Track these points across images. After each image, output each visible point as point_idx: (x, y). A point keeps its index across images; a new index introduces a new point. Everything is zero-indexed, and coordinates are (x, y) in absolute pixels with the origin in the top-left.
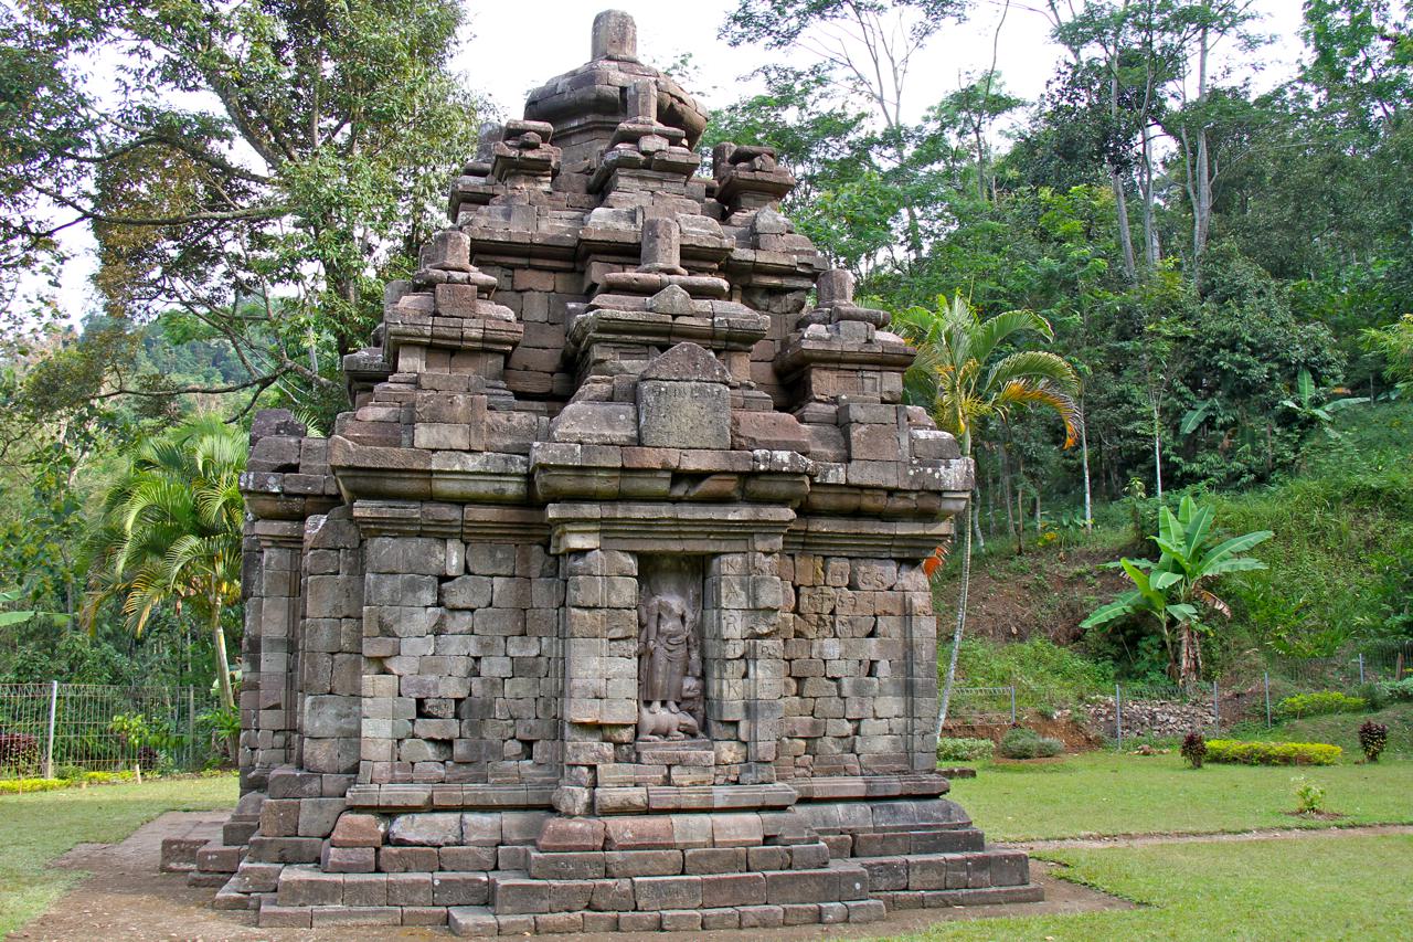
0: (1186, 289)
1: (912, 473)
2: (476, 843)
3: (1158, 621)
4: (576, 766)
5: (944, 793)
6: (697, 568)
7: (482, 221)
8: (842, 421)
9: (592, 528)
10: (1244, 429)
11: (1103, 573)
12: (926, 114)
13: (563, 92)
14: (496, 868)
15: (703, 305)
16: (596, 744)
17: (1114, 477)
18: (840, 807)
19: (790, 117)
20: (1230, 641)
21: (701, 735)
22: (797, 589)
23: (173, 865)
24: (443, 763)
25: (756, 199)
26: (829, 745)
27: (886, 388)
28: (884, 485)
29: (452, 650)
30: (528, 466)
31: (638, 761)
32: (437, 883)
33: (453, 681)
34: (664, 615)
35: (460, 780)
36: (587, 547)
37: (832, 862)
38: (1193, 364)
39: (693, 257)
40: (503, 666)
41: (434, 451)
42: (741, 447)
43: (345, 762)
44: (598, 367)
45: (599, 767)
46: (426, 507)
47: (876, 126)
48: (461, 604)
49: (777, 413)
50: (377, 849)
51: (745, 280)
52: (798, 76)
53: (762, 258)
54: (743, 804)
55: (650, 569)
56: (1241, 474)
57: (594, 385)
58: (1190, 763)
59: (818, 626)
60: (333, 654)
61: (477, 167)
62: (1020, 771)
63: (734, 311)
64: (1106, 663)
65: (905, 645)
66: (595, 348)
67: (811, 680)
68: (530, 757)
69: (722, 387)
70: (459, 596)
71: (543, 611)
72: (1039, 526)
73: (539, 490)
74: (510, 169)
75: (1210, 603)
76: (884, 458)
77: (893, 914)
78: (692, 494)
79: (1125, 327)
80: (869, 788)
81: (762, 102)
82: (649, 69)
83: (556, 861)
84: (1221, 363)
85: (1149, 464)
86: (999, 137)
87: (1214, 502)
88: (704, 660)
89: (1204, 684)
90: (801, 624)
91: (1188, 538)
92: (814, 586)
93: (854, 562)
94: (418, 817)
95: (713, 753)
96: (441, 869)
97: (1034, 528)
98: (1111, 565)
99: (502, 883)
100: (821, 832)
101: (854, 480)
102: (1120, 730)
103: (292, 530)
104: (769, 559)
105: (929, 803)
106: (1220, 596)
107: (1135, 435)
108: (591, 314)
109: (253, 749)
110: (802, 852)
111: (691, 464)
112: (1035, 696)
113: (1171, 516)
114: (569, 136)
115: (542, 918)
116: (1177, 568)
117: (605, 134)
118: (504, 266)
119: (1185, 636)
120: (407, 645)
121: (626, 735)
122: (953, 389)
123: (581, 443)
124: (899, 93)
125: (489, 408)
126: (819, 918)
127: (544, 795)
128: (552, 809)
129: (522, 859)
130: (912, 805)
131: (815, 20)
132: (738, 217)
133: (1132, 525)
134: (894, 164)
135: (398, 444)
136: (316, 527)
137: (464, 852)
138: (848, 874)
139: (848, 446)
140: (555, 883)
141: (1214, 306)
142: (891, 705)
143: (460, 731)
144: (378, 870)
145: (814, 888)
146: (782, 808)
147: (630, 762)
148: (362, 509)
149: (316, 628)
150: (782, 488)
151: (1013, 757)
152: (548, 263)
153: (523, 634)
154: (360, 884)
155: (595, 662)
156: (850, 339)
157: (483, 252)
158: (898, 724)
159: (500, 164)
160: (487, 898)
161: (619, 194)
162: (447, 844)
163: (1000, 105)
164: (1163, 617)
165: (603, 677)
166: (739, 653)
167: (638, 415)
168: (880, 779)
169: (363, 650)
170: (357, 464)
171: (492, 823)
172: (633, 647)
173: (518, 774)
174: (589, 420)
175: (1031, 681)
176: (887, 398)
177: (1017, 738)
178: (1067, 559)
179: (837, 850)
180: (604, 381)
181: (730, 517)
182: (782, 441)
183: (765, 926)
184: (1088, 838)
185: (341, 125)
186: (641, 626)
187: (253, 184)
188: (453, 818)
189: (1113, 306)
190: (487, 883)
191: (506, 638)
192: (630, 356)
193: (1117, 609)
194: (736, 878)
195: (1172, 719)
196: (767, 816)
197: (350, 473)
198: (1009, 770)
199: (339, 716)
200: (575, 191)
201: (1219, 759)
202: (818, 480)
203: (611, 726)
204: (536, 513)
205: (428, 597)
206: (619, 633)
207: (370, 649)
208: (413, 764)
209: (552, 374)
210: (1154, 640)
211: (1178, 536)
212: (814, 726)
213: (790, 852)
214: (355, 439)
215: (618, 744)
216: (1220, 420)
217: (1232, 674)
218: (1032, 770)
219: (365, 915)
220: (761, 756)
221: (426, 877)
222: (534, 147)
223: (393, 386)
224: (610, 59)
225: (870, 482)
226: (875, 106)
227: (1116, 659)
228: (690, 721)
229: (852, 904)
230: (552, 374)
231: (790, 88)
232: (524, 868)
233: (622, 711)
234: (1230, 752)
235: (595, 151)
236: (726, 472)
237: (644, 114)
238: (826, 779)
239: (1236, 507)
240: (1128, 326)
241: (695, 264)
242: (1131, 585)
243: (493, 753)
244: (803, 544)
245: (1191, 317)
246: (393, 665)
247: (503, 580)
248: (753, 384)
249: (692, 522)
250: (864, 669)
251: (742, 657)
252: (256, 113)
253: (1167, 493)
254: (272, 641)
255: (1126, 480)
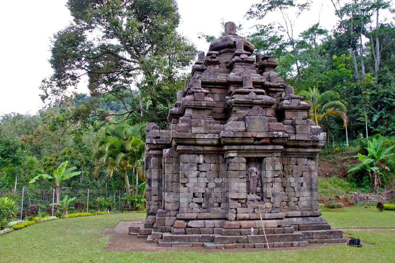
0: (373, 81)
1: (311, 136)
2: (208, 227)
3: (368, 172)
4: (232, 209)
5: (320, 215)
6: (259, 161)
7: (203, 77)
8: (293, 124)
9: (235, 151)
10: (391, 119)
11: (352, 159)
12: (300, 35)
13: (220, 43)
14: (213, 233)
15: (260, 96)
16: (237, 204)
17: (354, 132)
18: (295, 219)
19: (264, 38)
20: (389, 177)
21: (261, 201)
22: (283, 165)
23: (132, 233)
24: (199, 208)
25: (269, 69)
26: (291, 203)
27: (304, 115)
28: (304, 140)
29: (201, 181)
30: (219, 137)
31: (247, 207)
32: (200, 237)
33: (202, 189)
34: (252, 172)
35: (204, 212)
36: (234, 156)
37: (294, 232)
38: (376, 101)
39: (256, 84)
40: (213, 185)
41: (197, 133)
42: (270, 131)
43: (176, 208)
44: (234, 112)
45: (238, 209)
46: (195, 147)
47: (286, 39)
48: (203, 170)
49: (278, 123)
50: (185, 229)
51: (269, 90)
52: (265, 27)
53: (271, 84)
54: (272, 218)
55: (249, 161)
56: (391, 131)
57: (233, 117)
58: (379, 210)
59: (289, 174)
60: (172, 182)
61: (199, 62)
62: (332, 211)
63: (266, 98)
64: (354, 183)
65: (310, 179)
66: (234, 108)
67: (287, 187)
68: (220, 207)
69: (265, 117)
70: (203, 168)
71: (223, 172)
72: (334, 146)
73: (222, 142)
74: (208, 63)
75: (383, 167)
76: (304, 133)
77: (310, 245)
78: (259, 143)
79: (356, 92)
80: (302, 214)
81: (258, 34)
82: (240, 37)
83: (229, 231)
84: (384, 101)
85: (364, 129)
86: (319, 40)
87: (383, 139)
88: (261, 183)
89: (382, 189)
90: (285, 174)
91: (376, 149)
92: (287, 165)
93: (297, 159)
94: (194, 221)
95: (265, 206)
96: (200, 233)
97: (332, 147)
98: (354, 156)
99: (216, 236)
100: (292, 225)
101: (297, 139)
102: (358, 201)
103: (159, 152)
104: (277, 158)
105: (317, 218)
106: (386, 165)
107: (360, 121)
108: (233, 100)
109: (150, 205)
110: (287, 229)
111: (259, 136)
112: (335, 192)
113: (371, 143)
114: (221, 54)
115: (226, 245)
116: (373, 157)
117: (231, 53)
118: (208, 87)
119: (376, 176)
120: (190, 180)
121: (243, 201)
122: (314, 112)
123: (232, 131)
124: (292, 31)
125: (209, 123)
126: (292, 245)
127: (224, 216)
128: (226, 219)
129: (219, 231)
130: (313, 218)
131: (269, 11)
132: (264, 73)
133: (360, 146)
134: (292, 49)
135: (188, 132)
136: (166, 152)
137: (206, 230)
138: (298, 235)
139: (295, 130)
140: (229, 236)
141: (382, 85)
142: (307, 194)
143: (204, 200)
144: (186, 234)
145: (290, 238)
146: (282, 219)
147: (245, 207)
148: (179, 148)
149: (168, 176)
150: (280, 141)
151: (330, 208)
152: (219, 87)
153: (218, 177)
154: (182, 237)
155: (236, 184)
156: (294, 104)
157: (205, 84)
158: (309, 198)
159: (206, 62)
160: (212, 240)
161: (236, 69)
162: (201, 228)
163: (321, 32)
164: (369, 171)
165: (238, 187)
166: (271, 181)
167: (245, 124)
168: (304, 212)
169: (179, 180)
170: (179, 137)
171: (212, 223)
172: (245, 180)
173: (217, 211)
174: (234, 125)
175: (333, 188)
176: (304, 118)
177: (331, 203)
178: (342, 155)
179: (295, 229)
180: (236, 116)
181: (268, 148)
182: (280, 130)
183: (279, 247)
184: (354, 228)
185: (152, 46)
186: (247, 175)
187: (127, 62)
188: (202, 221)
189: (353, 86)
190: (212, 237)
191: (214, 178)
192: (242, 109)
193: (357, 167)
194: (272, 236)
195: (373, 198)
196: (278, 221)
197: (177, 139)
198: (329, 211)
199: (174, 197)
200: (224, 68)
201: (387, 209)
202: (288, 139)
203: (240, 199)
204: (221, 148)
205: (195, 168)
206: (242, 177)
207: (182, 181)
208: (192, 208)
209: (221, 114)
210: (367, 177)
211: (373, 149)
212: (288, 199)
213: (284, 229)
214: (177, 131)
215: (242, 203)
216: (384, 117)
217: (390, 186)
218: (336, 211)
219: (184, 244)
220: (276, 206)
221: (197, 235)
222: (214, 58)
223: (185, 118)
224: (230, 34)
225: (301, 139)
226: (285, 34)
227: (356, 182)
228: (259, 198)
229: (300, 242)
230: (221, 114)
231: (263, 30)
232: (220, 233)
233: (243, 195)
234: (391, 207)
235: (226, 58)
236: (267, 138)
237: (241, 49)
238: (291, 212)
239: (389, 140)
240: (358, 91)
241: (256, 86)
242: (360, 162)
243: (212, 206)
244: (285, 154)
245: (375, 89)
246: (187, 185)
247: (213, 164)
248: (272, 116)
249: (259, 150)
250: (300, 185)
251: (271, 182)
252: (129, 44)
253: (369, 137)
254: (154, 179)
255: (358, 134)
